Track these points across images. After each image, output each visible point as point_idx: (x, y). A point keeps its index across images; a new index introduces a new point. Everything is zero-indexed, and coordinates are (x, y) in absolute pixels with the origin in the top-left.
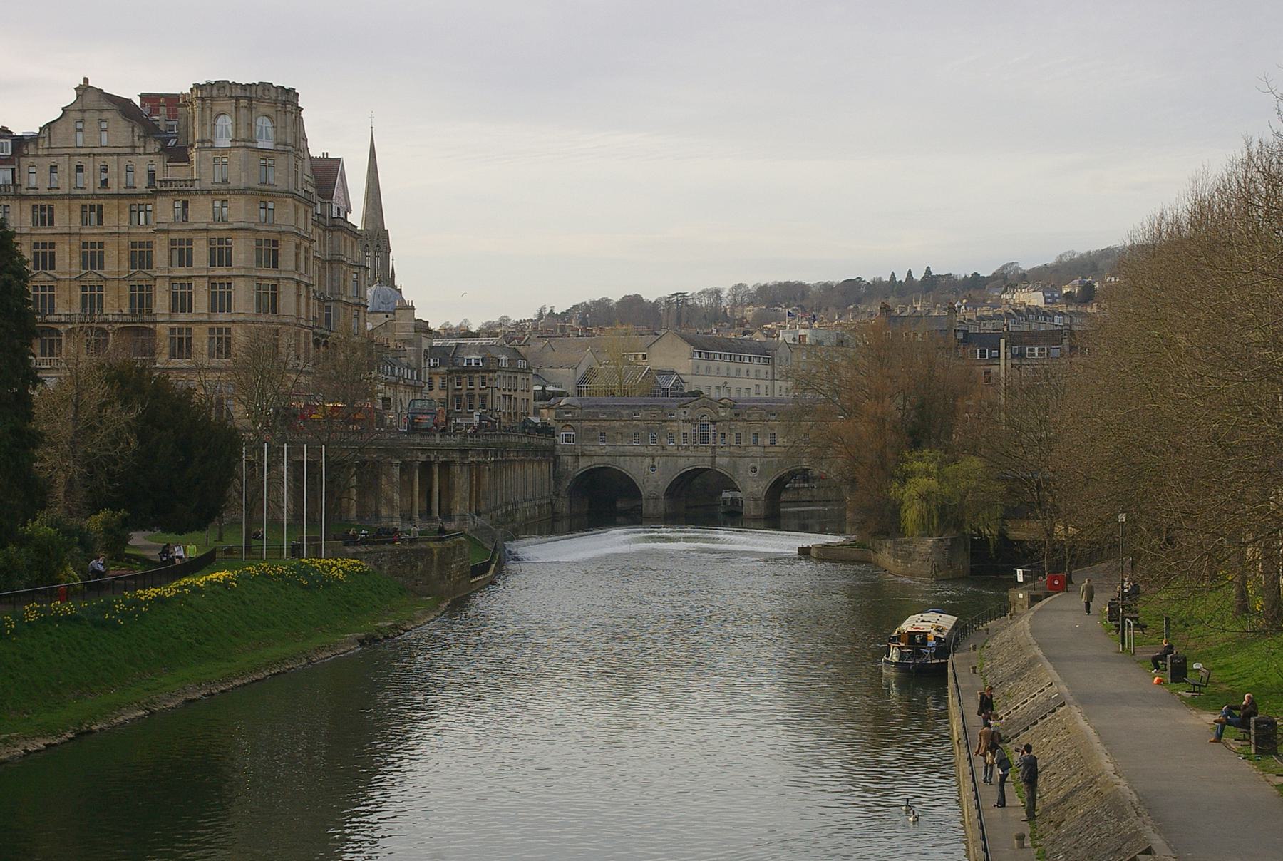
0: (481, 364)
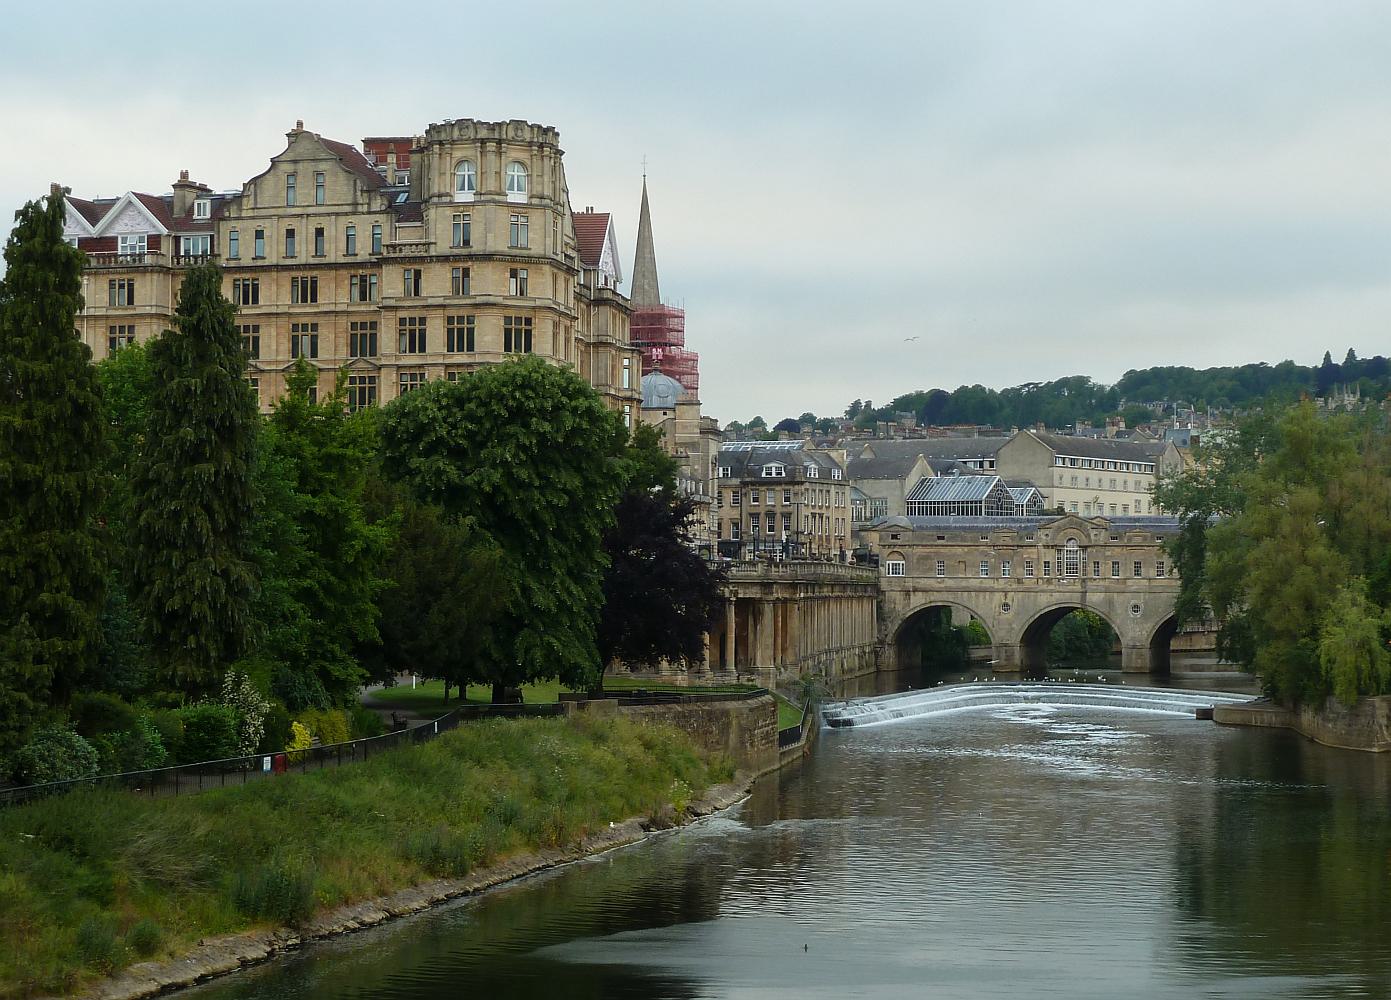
0: (784, 475)
